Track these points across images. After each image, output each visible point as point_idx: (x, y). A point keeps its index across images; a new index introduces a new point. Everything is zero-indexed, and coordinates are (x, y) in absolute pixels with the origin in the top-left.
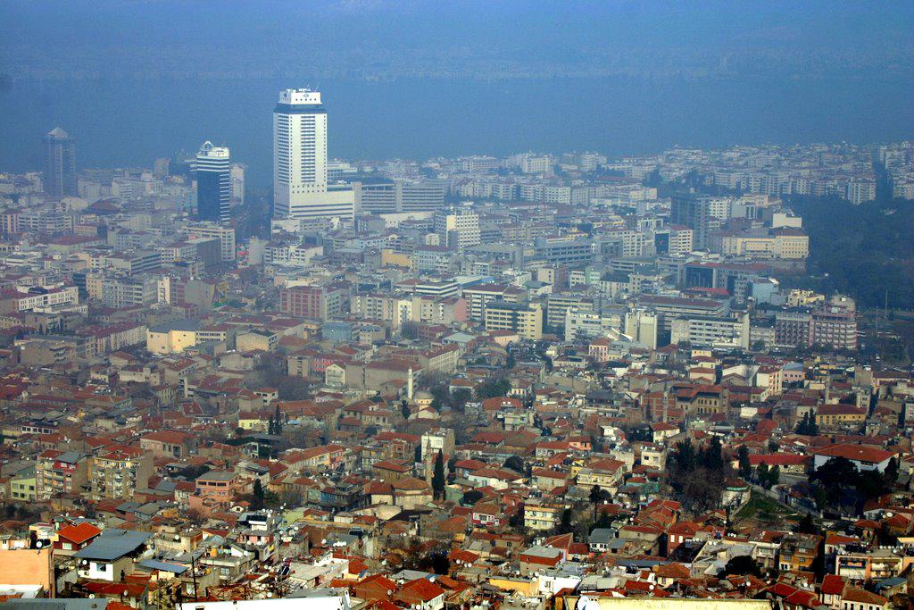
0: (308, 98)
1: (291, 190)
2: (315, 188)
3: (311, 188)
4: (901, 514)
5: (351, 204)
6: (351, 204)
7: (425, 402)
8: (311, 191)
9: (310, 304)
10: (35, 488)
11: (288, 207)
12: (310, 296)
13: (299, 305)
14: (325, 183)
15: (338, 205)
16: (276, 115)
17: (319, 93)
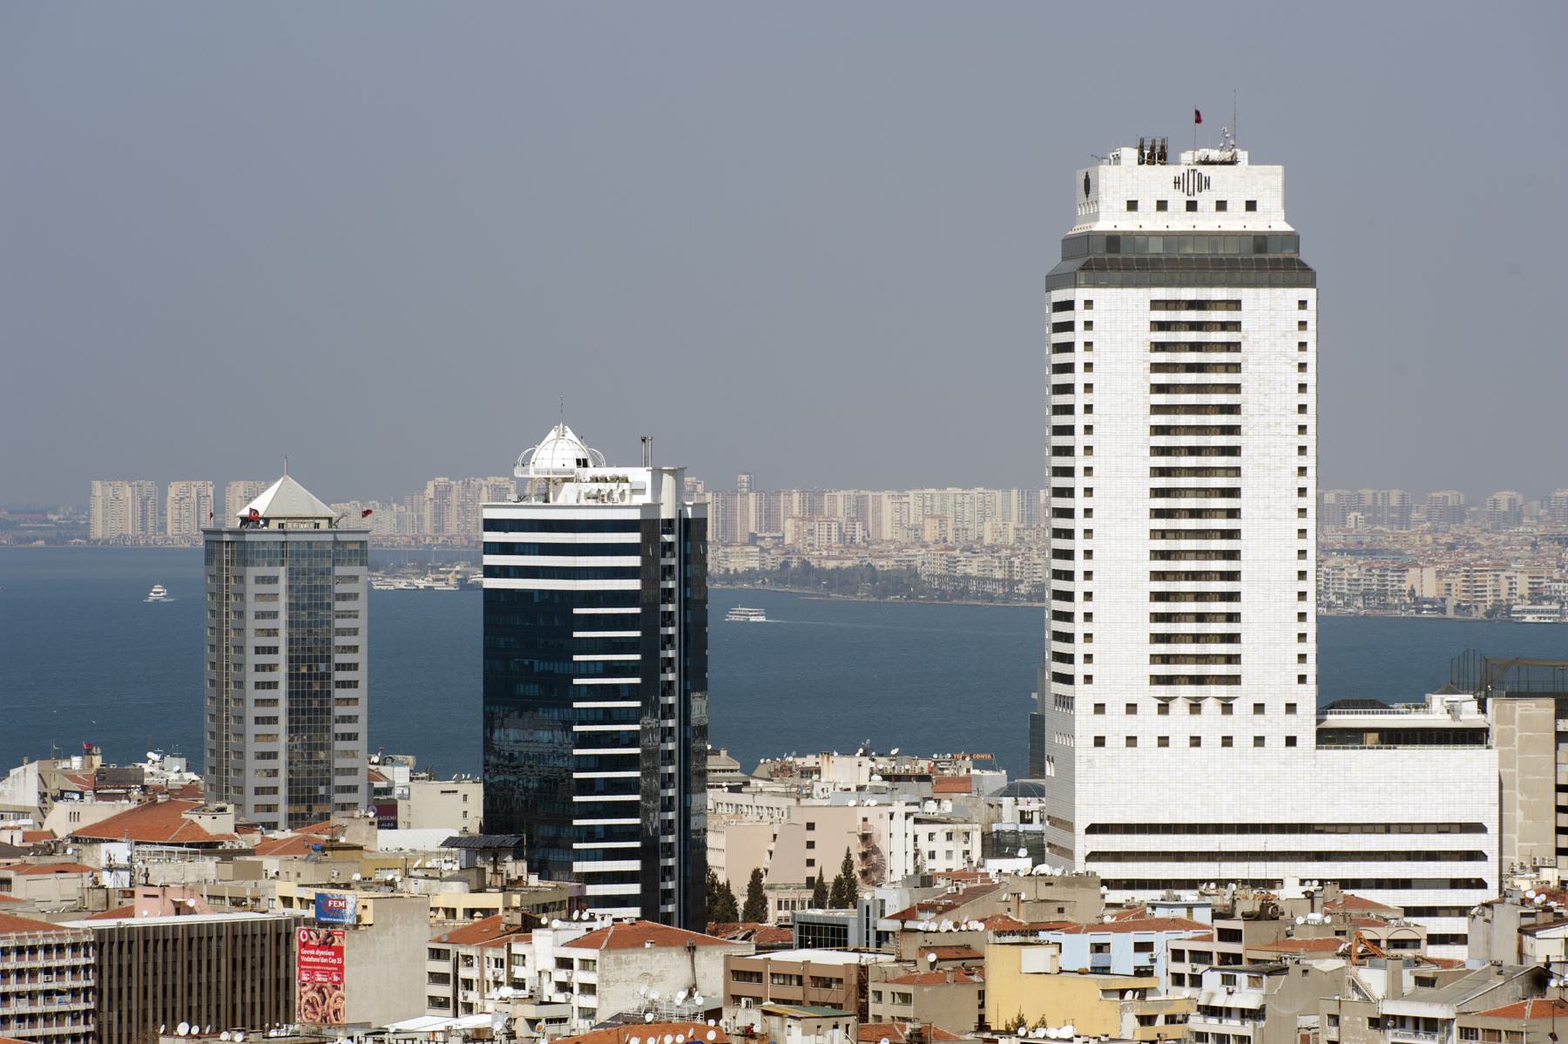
0: (1206, 200)
1: (1085, 724)
2: (1242, 724)
3: (1211, 722)
5: (1479, 828)
6: (1479, 828)
8: (1212, 740)
10: (1100, 938)
11: (1069, 826)
14: (1307, 697)
15: (1387, 828)
17: (1279, 169)
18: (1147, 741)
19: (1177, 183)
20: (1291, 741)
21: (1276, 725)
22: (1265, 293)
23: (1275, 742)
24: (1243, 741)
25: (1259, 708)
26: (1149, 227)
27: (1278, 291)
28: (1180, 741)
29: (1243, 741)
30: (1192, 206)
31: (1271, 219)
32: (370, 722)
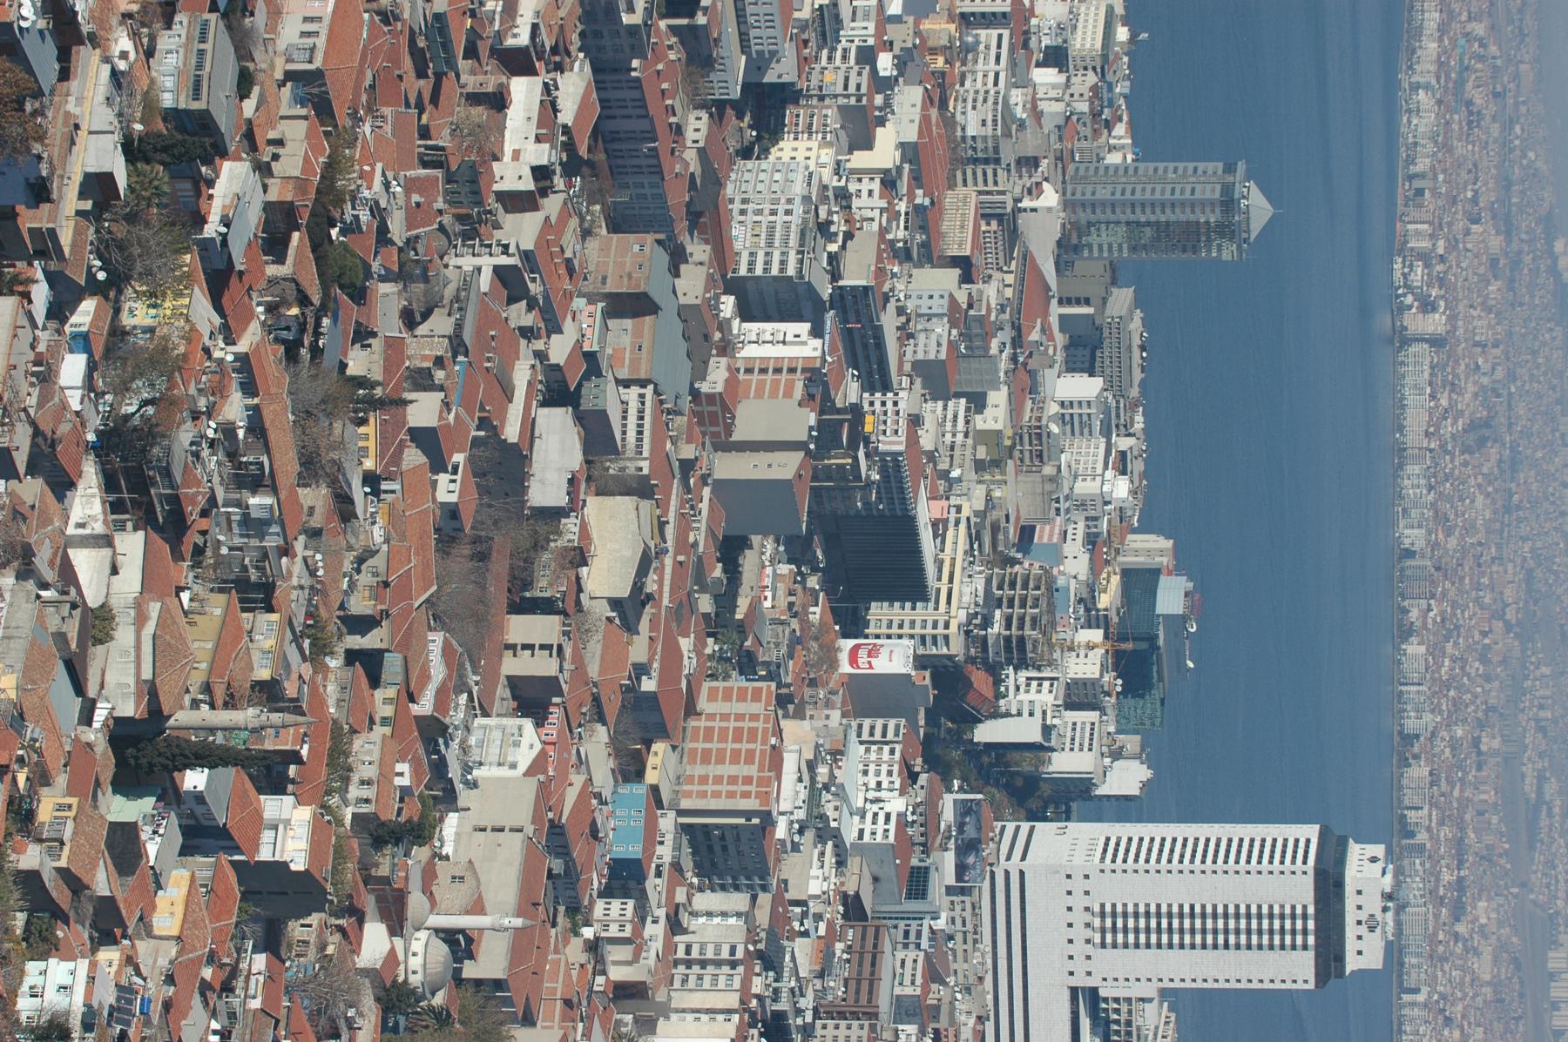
2: (1079, 949)
3: (1080, 933)
4: (307, 653)
7: (415, 963)
8: (1071, 933)
9: (727, 770)
12: (752, 771)
13: (723, 739)
16: (1311, 832)
17: (1380, 967)
18: (1070, 901)
19: (1372, 916)
20: (1071, 973)
21: (1080, 966)
22: (1312, 963)
23: (1070, 966)
24: (1071, 949)
25: (1089, 957)
26: (1347, 902)
27: (1313, 970)
28: (1070, 917)
29: (1071, 949)
30: (1359, 923)
31: (1352, 963)
32: (1236, 990)
